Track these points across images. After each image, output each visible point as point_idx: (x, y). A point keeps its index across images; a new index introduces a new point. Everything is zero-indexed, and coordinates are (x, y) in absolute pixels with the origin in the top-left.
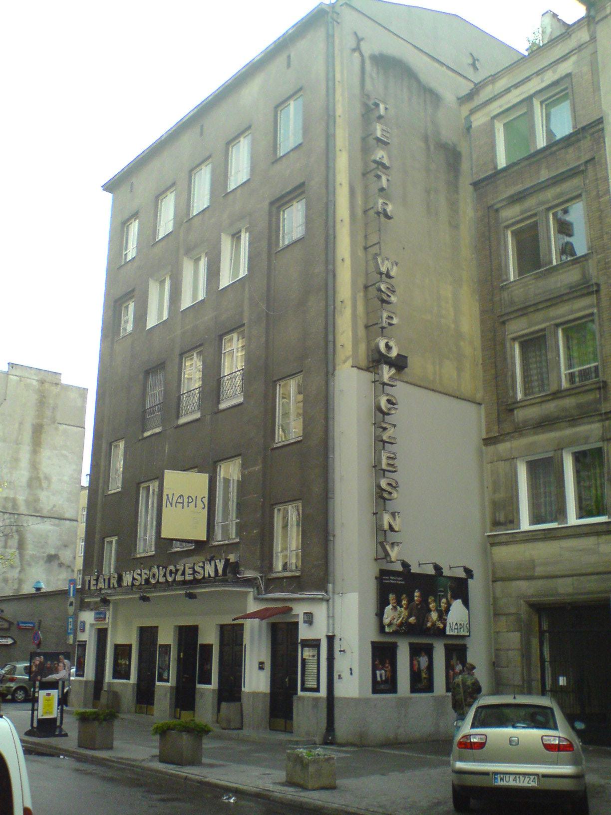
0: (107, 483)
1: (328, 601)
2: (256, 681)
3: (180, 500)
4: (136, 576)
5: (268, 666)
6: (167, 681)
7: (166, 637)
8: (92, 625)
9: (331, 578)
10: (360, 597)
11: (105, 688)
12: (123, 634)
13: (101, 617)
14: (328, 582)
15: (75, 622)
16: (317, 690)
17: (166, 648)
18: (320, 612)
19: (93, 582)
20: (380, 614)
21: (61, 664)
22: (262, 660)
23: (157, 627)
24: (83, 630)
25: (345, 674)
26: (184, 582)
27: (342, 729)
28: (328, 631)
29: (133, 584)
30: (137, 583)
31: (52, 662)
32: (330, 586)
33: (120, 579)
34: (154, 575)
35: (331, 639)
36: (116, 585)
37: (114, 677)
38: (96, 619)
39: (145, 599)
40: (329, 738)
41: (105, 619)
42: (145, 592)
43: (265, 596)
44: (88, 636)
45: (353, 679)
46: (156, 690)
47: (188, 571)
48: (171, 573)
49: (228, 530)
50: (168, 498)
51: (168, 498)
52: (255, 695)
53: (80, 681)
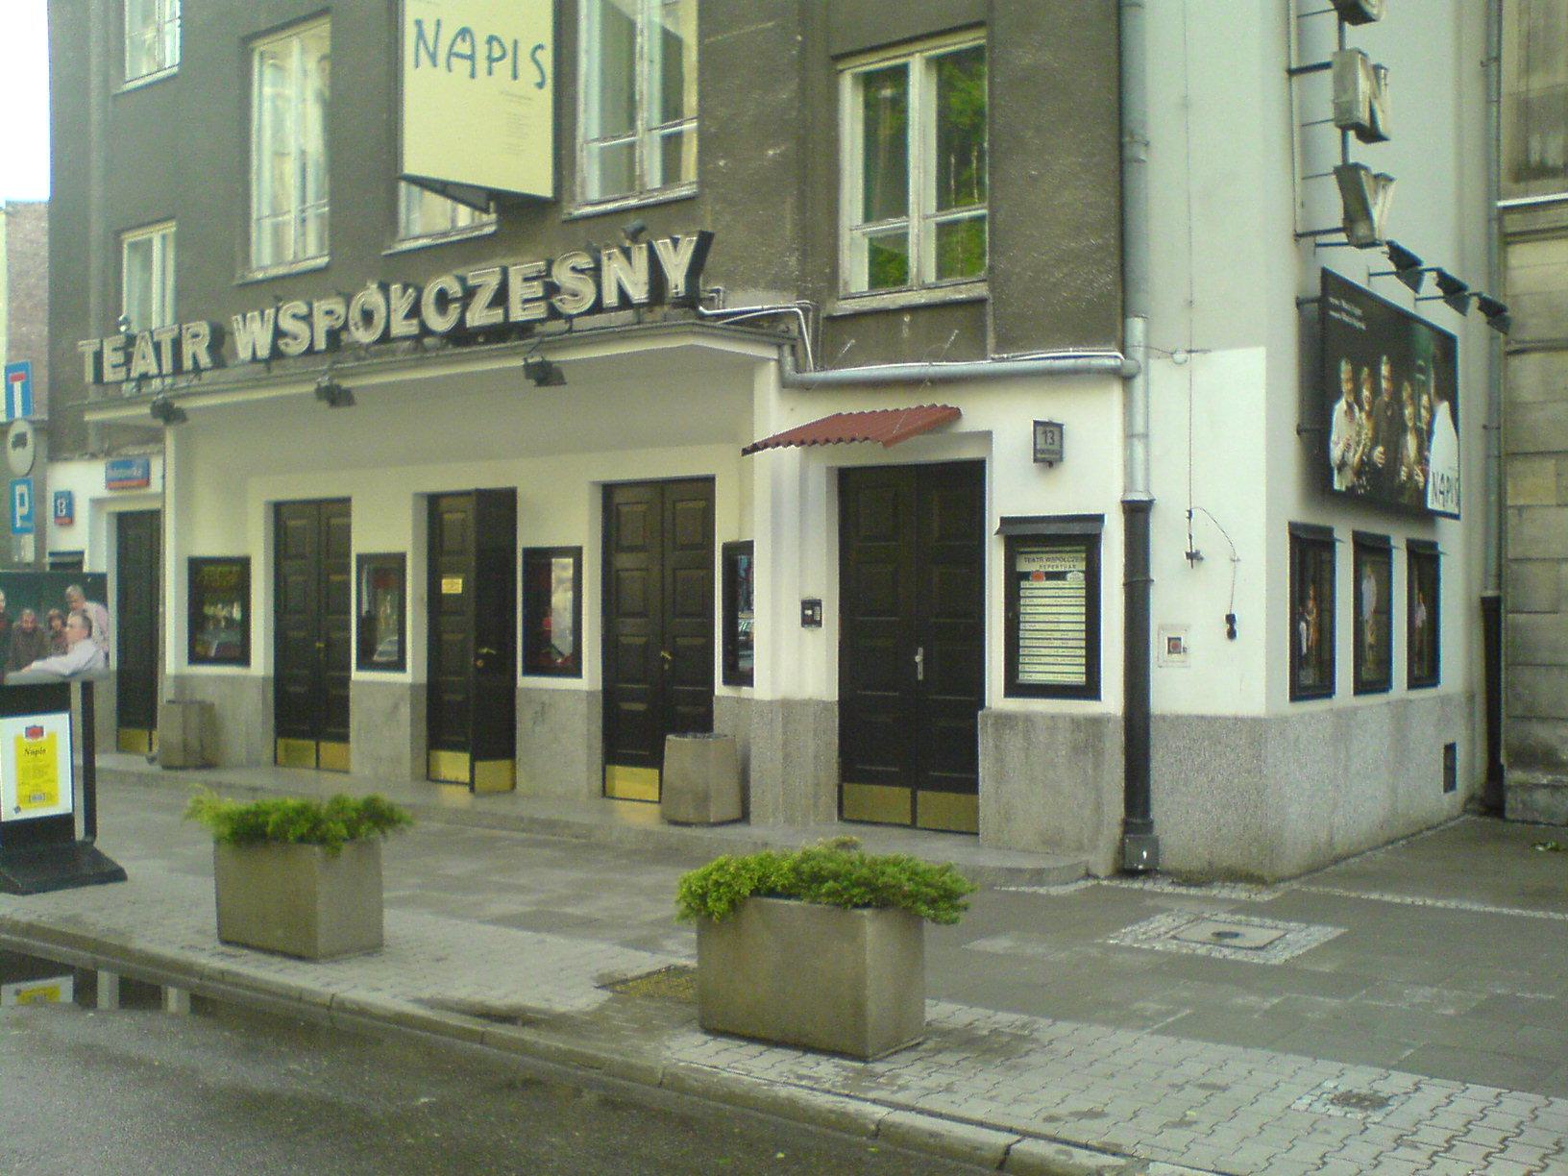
0: (115, 54)
1: (1126, 378)
2: (793, 660)
3: (463, 48)
4: (287, 324)
5: (830, 613)
6: (399, 665)
7: (384, 528)
8: (97, 503)
9: (1139, 300)
10: (1269, 356)
11: (166, 692)
12: (216, 521)
13: (127, 476)
14: (1125, 312)
15: (38, 497)
16: (1090, 689)
17: (386, 571)
18: (1093, 421)
19: (111, 358)
20: (1314, 431)
21: (74, 620)
22: (812, 593)
23: (346, 501)
24: (67, 519)
25: (1203, 633)
26: (501, 333)
27: (1182, 819)
28: (1129, 486)
29: (276, 353)
30: (294, 348)
31: (37, 607)
32: (1137, 327)
33: (219, 340)
34: (368, 317)
35: (1137, 513)
36: (205, 360)
37: (195, 658)
38: (111, 484)
39: (335, 397)
40: (1137, 857)
41: (146, 481)
42: (334, 373)
43: (821, 375)
44: (88, 540)
45: (1221, 653)
46: (352, 693)
47: (518, 290)
48: (443, 300)
49: (657, 153)
50: (421, 36)
51: (421, 36)
52: (788, 708)
53: (1077, 723)
